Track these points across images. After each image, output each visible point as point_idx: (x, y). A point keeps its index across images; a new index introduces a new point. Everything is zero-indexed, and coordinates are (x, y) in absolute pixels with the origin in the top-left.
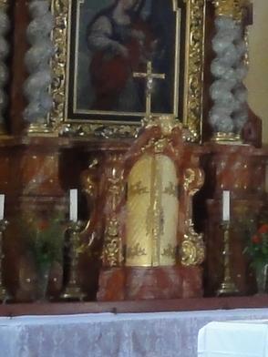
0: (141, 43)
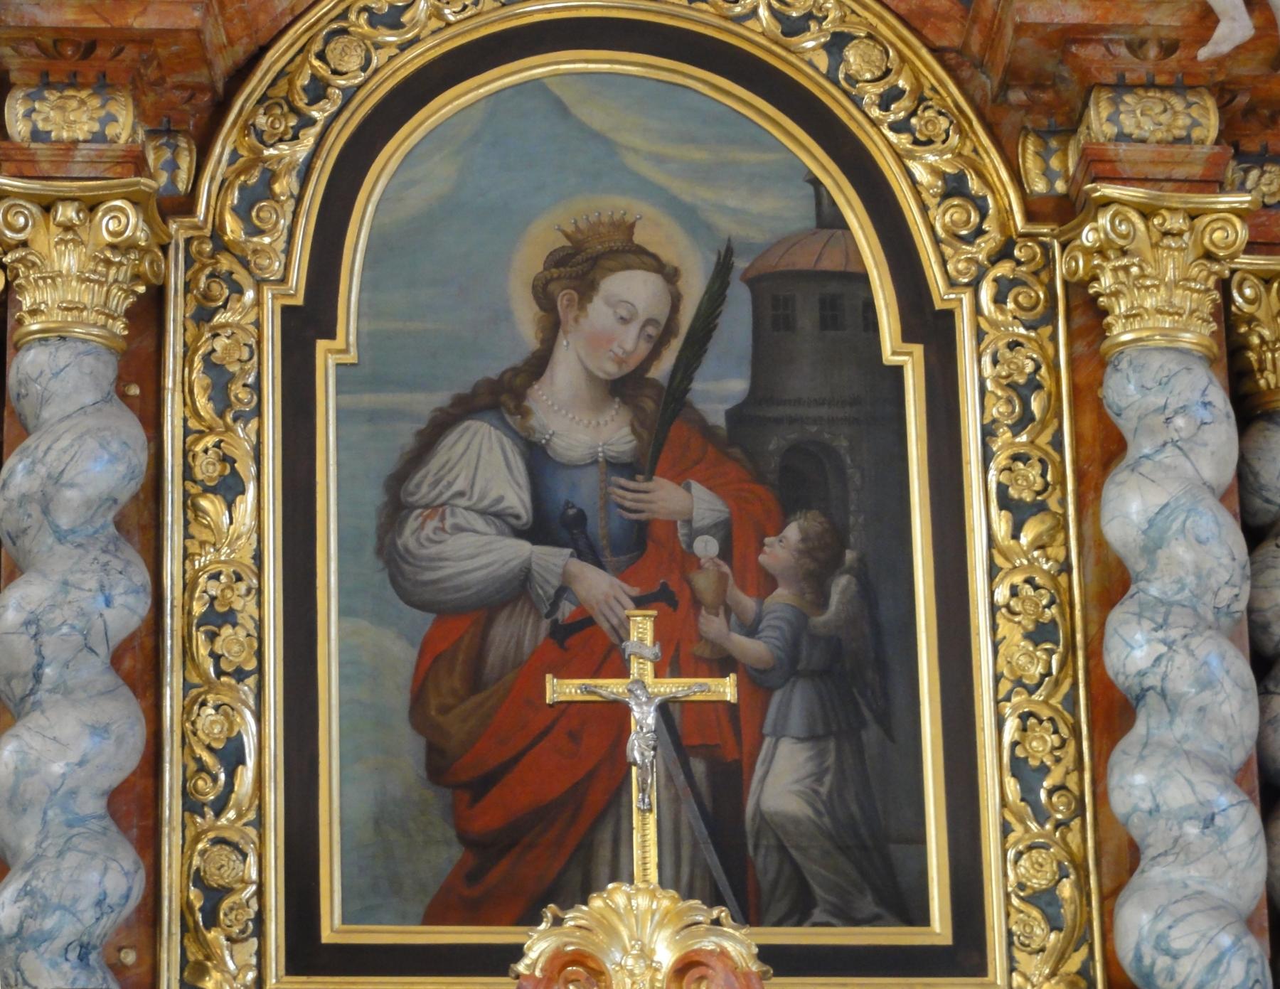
0: (707, 547)
